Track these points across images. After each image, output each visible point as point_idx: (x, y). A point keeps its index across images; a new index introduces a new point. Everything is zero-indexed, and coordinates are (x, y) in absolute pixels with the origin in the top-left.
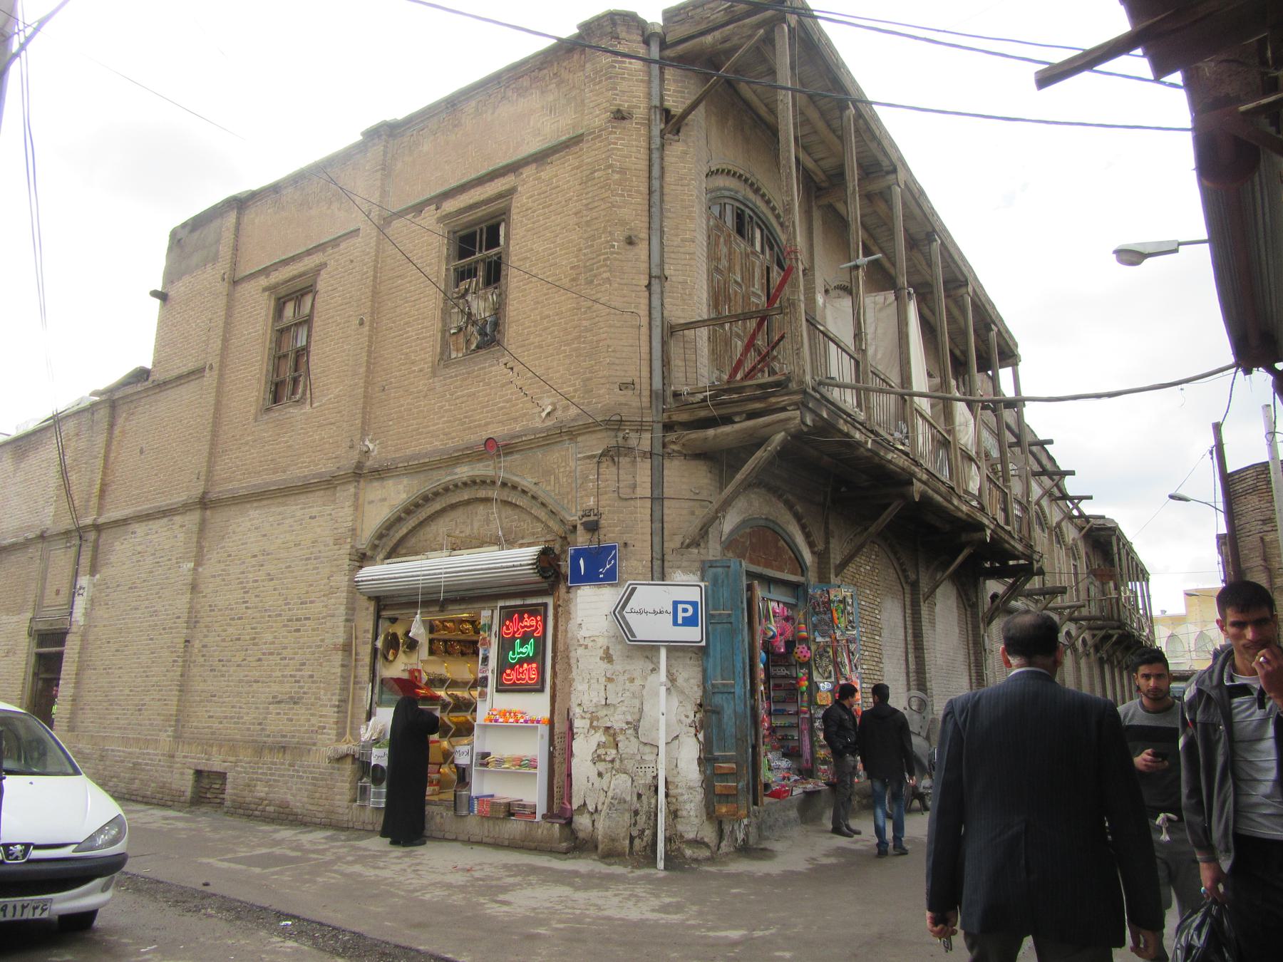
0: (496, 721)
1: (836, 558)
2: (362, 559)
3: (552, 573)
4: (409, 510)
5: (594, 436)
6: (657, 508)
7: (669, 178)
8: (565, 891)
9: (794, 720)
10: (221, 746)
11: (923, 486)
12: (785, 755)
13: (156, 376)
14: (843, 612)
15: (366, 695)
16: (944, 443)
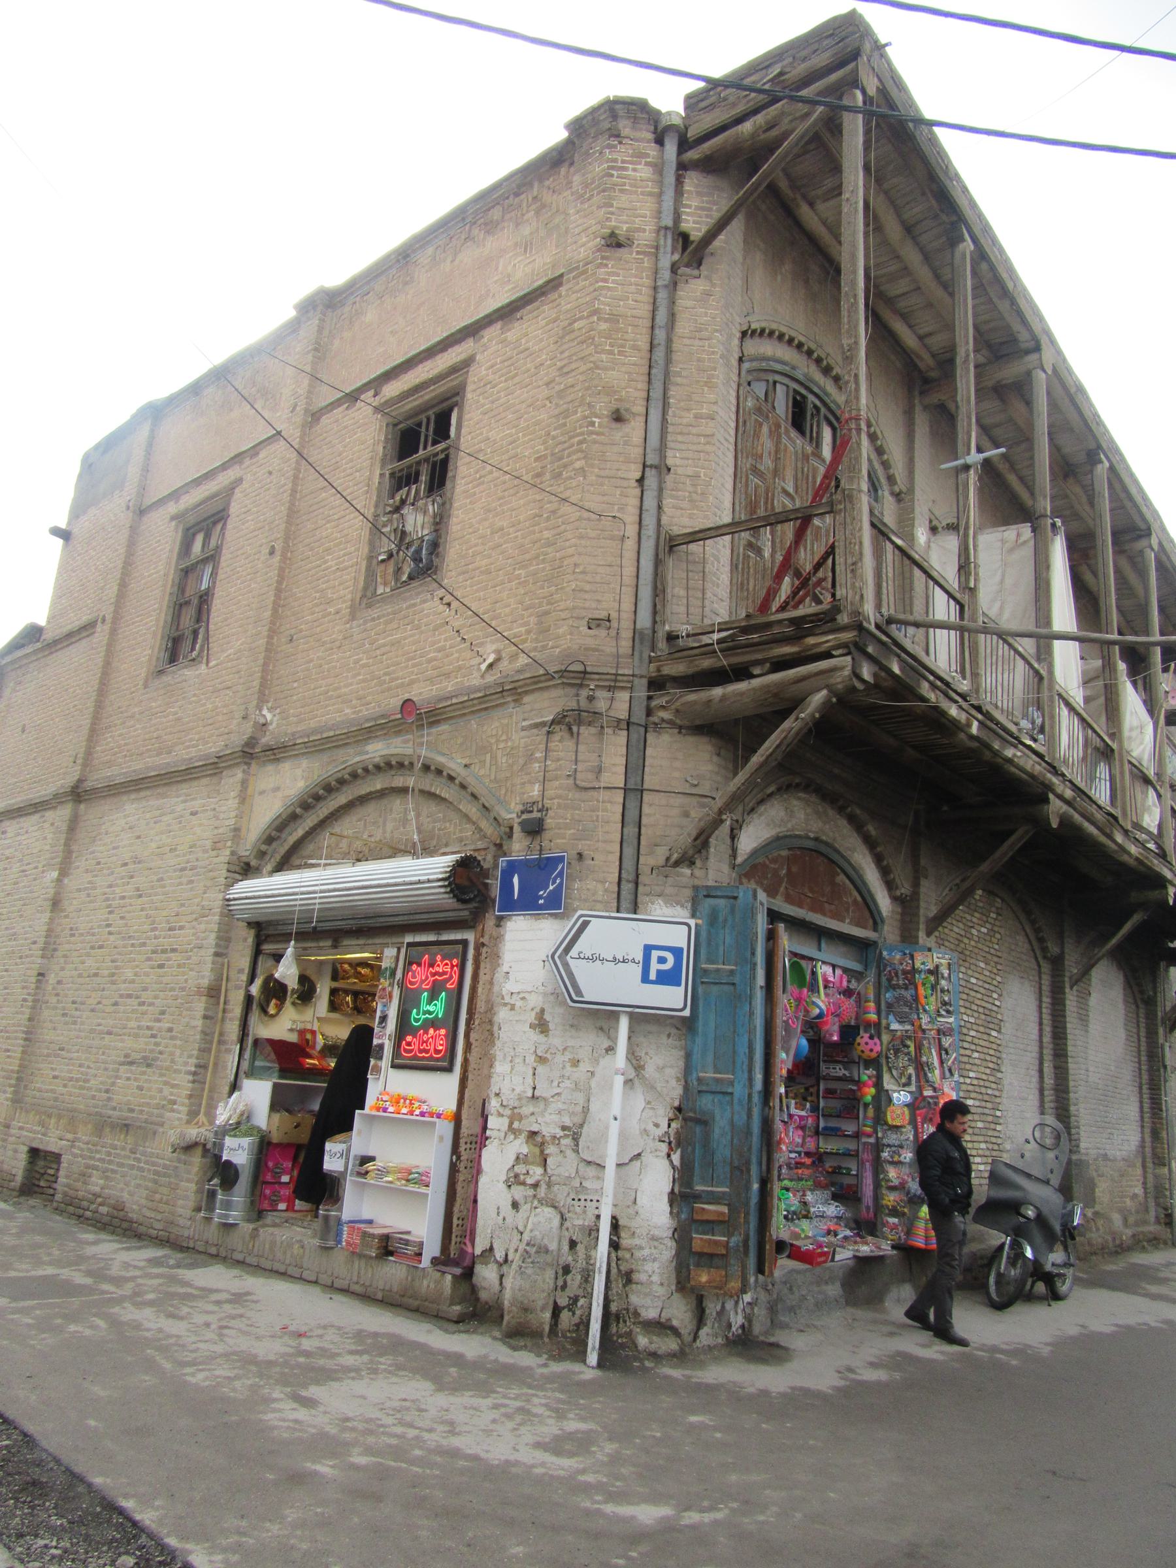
0: (385, 1110)
1: (929, 906)
2: (247, 870)
3: (473, 894)
4: (309, 801)
5: (546, 694)
6: (632, 805)
7: (683, 327)
8: (417, 1389)
9: (851, 1145)
10: (60, 1117)
11: (1065, 808)
12: (835, 1197)
13: (48, 636)
14: (933, 988)
15: (232, 1060)
16: (1105, 751)
